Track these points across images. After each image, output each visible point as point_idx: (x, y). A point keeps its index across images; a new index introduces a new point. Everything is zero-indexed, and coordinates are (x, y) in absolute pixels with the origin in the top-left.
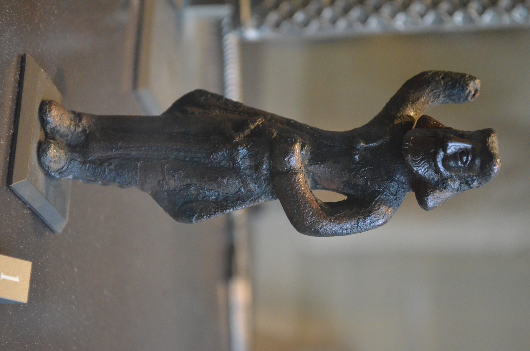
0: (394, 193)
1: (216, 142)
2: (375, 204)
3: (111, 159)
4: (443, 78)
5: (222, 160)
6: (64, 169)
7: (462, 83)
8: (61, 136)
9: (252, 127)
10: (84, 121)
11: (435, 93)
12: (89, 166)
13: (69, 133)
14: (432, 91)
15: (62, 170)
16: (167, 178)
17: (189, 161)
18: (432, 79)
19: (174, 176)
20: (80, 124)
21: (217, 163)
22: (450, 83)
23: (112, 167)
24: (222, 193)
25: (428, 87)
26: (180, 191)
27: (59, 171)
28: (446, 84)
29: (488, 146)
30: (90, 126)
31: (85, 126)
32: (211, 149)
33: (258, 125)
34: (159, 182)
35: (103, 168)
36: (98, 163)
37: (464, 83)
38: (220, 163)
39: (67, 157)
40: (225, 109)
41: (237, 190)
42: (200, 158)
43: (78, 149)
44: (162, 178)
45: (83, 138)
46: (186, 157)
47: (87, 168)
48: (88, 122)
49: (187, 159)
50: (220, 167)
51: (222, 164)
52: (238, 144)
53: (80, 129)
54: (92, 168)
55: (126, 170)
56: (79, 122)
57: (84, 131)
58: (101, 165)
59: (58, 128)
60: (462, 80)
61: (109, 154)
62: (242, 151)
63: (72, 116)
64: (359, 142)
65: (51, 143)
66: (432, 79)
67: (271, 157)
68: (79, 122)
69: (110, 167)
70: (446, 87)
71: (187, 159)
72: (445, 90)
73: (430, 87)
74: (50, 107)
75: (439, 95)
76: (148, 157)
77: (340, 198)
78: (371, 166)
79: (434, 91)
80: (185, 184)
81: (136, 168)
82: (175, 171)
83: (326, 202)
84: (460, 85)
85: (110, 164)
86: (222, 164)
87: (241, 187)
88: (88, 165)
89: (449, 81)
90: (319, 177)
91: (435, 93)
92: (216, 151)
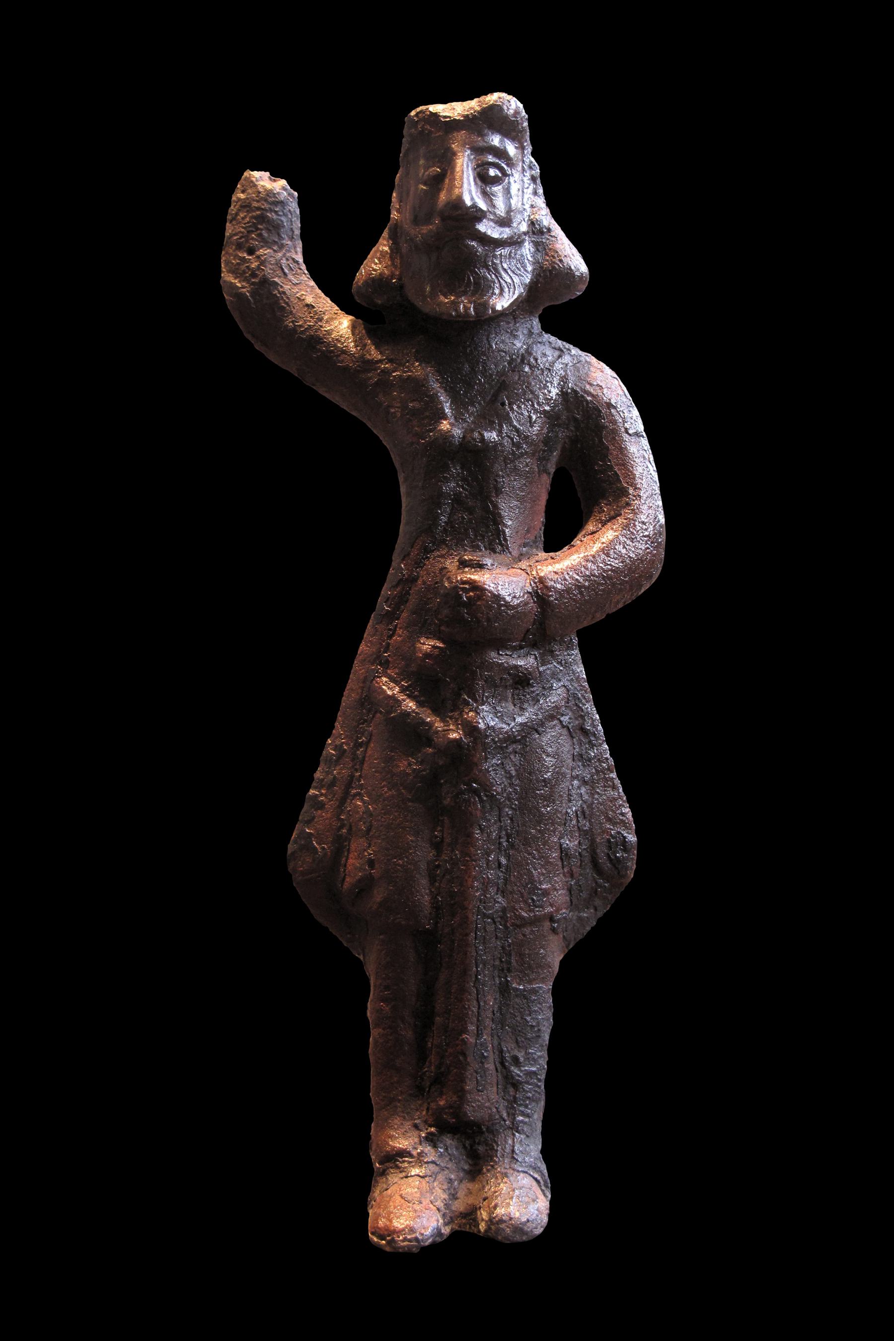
0: (557, 353)
1: (464, 787)
2: (589, 394)
3: (502, 1063)
4: (251, 252)
5: (506, 771)
6: (539, 1178)
7: (266, 206)
8: (454, 1197)
9: (412, 705)
11: (291, 269)
12: (523, 1114)
13: (441, 1177)
14: (285, 274)
17: (508, 857)
18: (254, 275)
19: (546, 893)
20: (414, 1153)
21: (511, 785)
22: (265, 234)
23: (521, 1056)
25: (277, 284)
26: (572, 876)
27: (543, 1188)
28: (266, 243)
30: (416, 1127)
31: (416, 1140)
33: (403, 690)
34: (554, 930)
35: (523, 1079)
36: (511, 1091)
37: (266, 200)
39: (510, 1171)
40: (349, 785)
41: (565, 732)
42: (500, 829)
43: (481, 1149)
44: (547, 924)
45: (448, 1140)
46: (500, 865)
49: (504, 861)
50: (519, 776)
51: (514, 773)
52: (471, 730)
53: (428, 1149)
54: (526, 1106)
55: (528, 1018)
56: (411, 1156)
57: (431, 1139)
58: (516, 1085)
59: (440, 1204)
60: (255, 204)
62: (487, 718)
65: (491, 1221)
66: (254, 275)
67: (500, 644)
68: (411, 1156)
70: (275, 243)
71: (504, 861)
72: (282, 247)
74: (400, 1232)
75: (293, 259)
76: (497, 963)
78: (503, 404)
79: (286, 271)
80: (560, 863)
81: (523, 995)
84: (271, 210)
85: (516, 1061)
86: (514, 773)
87: (561, 722)
88: (521, 1118)
89: (260, 235)
91: (291, 269)
92: (486, 787)
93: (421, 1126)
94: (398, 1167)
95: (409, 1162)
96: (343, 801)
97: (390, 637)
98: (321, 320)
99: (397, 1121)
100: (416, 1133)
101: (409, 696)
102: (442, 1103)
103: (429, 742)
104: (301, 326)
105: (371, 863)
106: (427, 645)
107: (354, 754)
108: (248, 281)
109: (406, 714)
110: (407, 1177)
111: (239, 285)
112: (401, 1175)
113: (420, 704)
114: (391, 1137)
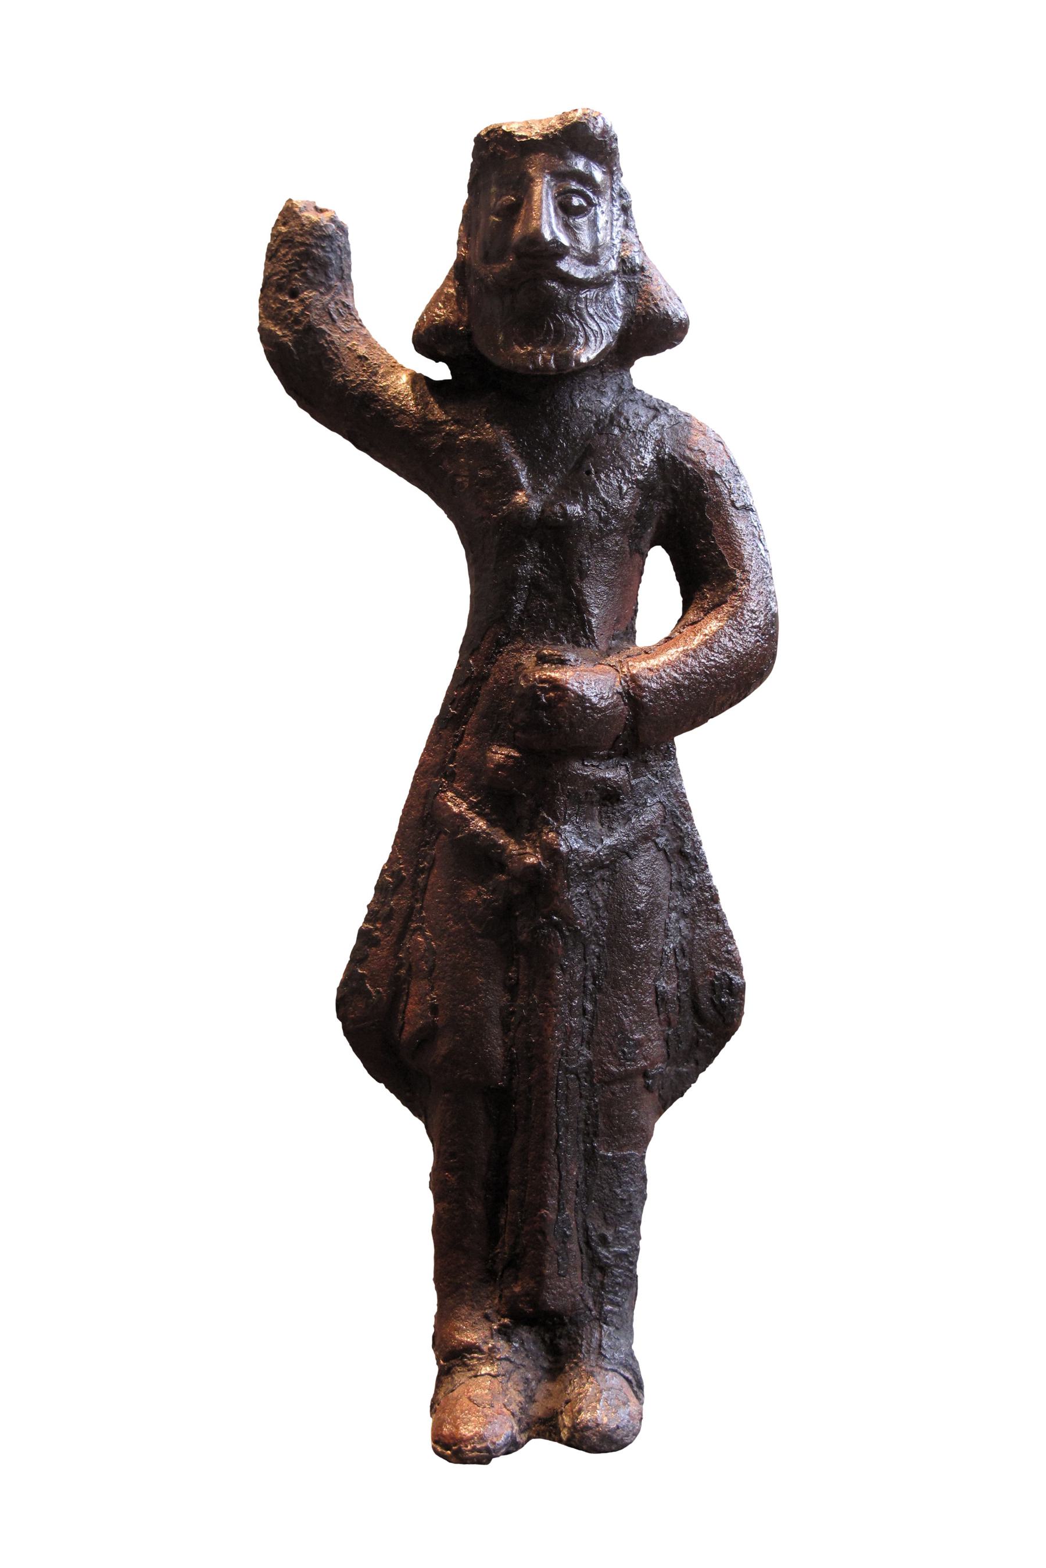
0: (652, 413)
1: (543, 920)
2: (689, 460)
4: (294, 294)
6: (631, 1378)
7: (312, 241)
8: (531, 1399)
9: (482, 824)
10: (470, 1337)
11: (340, 314)
12: (612, 1302)
13: (516, 1376)
14: (333, 320)
15: (634, 1383)
16: (643, 1063)
17: (595, 1002)
18: (297, 322)
19: (639, 1044)
20: (485, 1348)
23: (609, 1234)
24: (670, 899)
25: (324, 332)
26: (669, 1024)
27: (636, 1389)
28: (311, 285)
29: (546, 136)
30: (487, 1317)
31: (487, 1333)
32: (563, 936)
33: (471, 807)
36: (598, 1275)
37: (311, 234)
38: (598, 909)
39: (597, 1370)
40: (408, 918)
41: (661, 855)
43: (563, 1343)
44: (640, 1080)
45: (524, 1333)
46: (585, 1012)
47: (616, 1309)
48: (473, 1327)
49: (589, 1007)
51: (601, 904)
52: (551, 853)
53: (501, 1343)
54: (616, 1294)
55: (618, 1191)
57: (504, 1333)
58: (604, 1269)
59: (514, 1407)
60: (298, 239)
61: (573, 1247)
62: (570, 840)
63: (460, 1377)
64: (522, 511)
66: (297, 322)
67: (585, 754)
68: (481, 1351)
69: (610, 1239)
70: (322, 284)
71: (589, 1007)
72: (329, 288)
73: (323, 327)
75: (343, 303)
76: (582, 1125)
77: (658, 567)
78: (589, 473)
79: (335, 316)
81: (612, 1164)
82: (623, 1042)
83: (679, 600)
84: (317, 246)
85: (604, 1241)
86: (601, 904)
87: (656, 844)
88: (609, 1307)
89: (304, 275)
90: (618, 621)
91: (340, 314)
92: (569, 920)
93: (493, 1317)
94: (465, 1365)
95: (479, 1359)
96: (401, 937)
97: (457, 745)
98: (375, 374)
99: (464, 1311)
100: (486, 1325)
101: (479, 814)
102: (517, 1290)
103: (502, 868)
104: (352, 381)
105: (434, 1009)
106: (500, 754)
107: (415, 882)
108: (290, 329)
109: (476, 835)
110: (476, 1376)
111: (279, 333)
112: (470, 1374)
113: (491, 823)
114: (458, 1329)
